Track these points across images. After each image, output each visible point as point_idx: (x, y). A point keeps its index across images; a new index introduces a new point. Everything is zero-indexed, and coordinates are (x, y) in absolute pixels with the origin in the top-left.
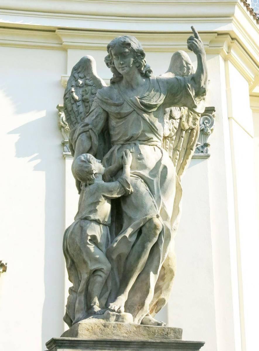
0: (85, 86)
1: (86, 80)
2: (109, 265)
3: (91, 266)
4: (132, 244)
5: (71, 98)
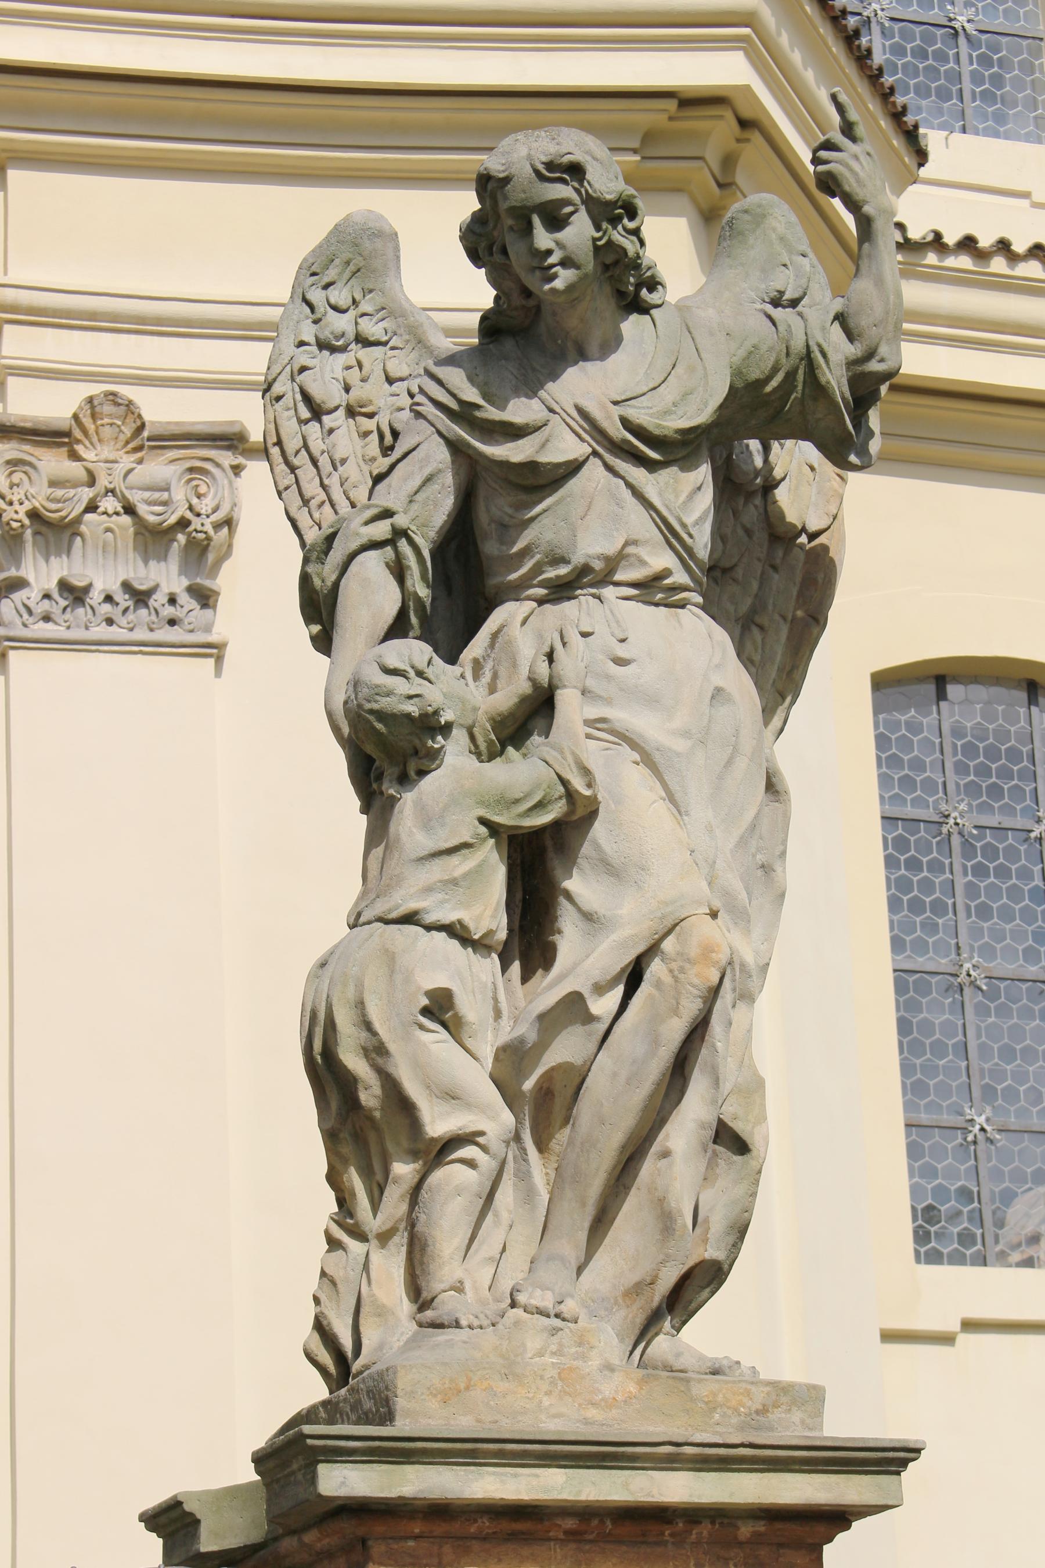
0: (353, 346)
1: (359, 320)
2: (508, 1118)
3: (433, 1122)
4: (603, 1027)
5: (299, 397)
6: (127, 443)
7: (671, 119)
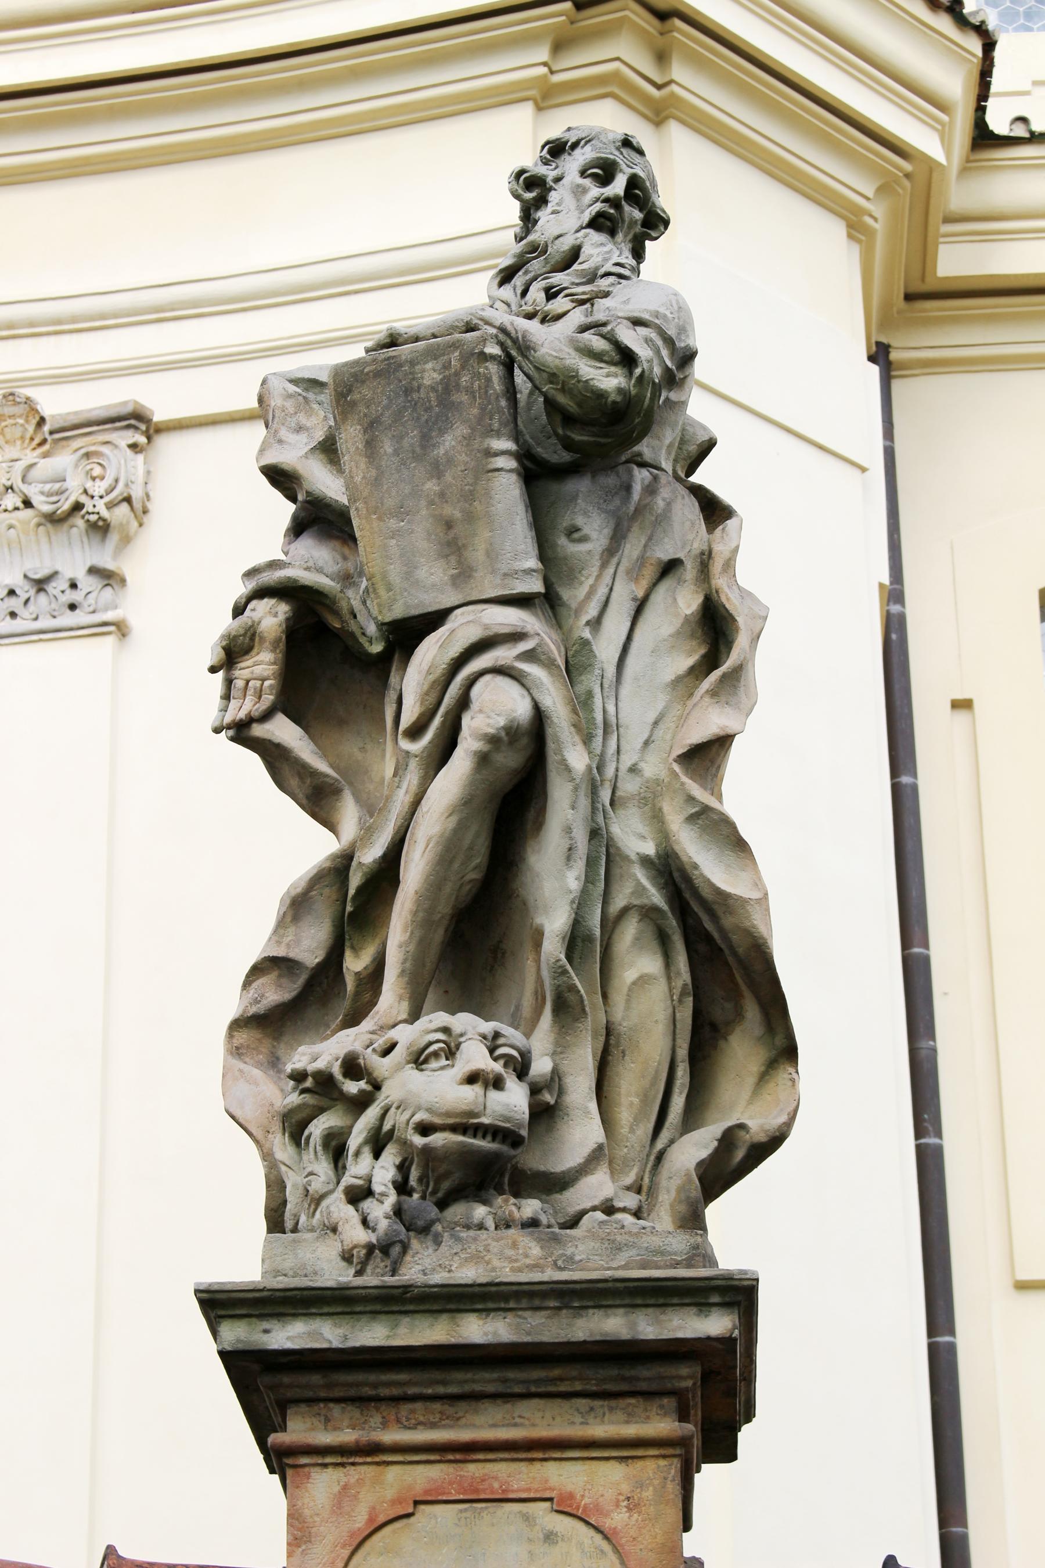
6: (32, 439)
7: (559, 47)
